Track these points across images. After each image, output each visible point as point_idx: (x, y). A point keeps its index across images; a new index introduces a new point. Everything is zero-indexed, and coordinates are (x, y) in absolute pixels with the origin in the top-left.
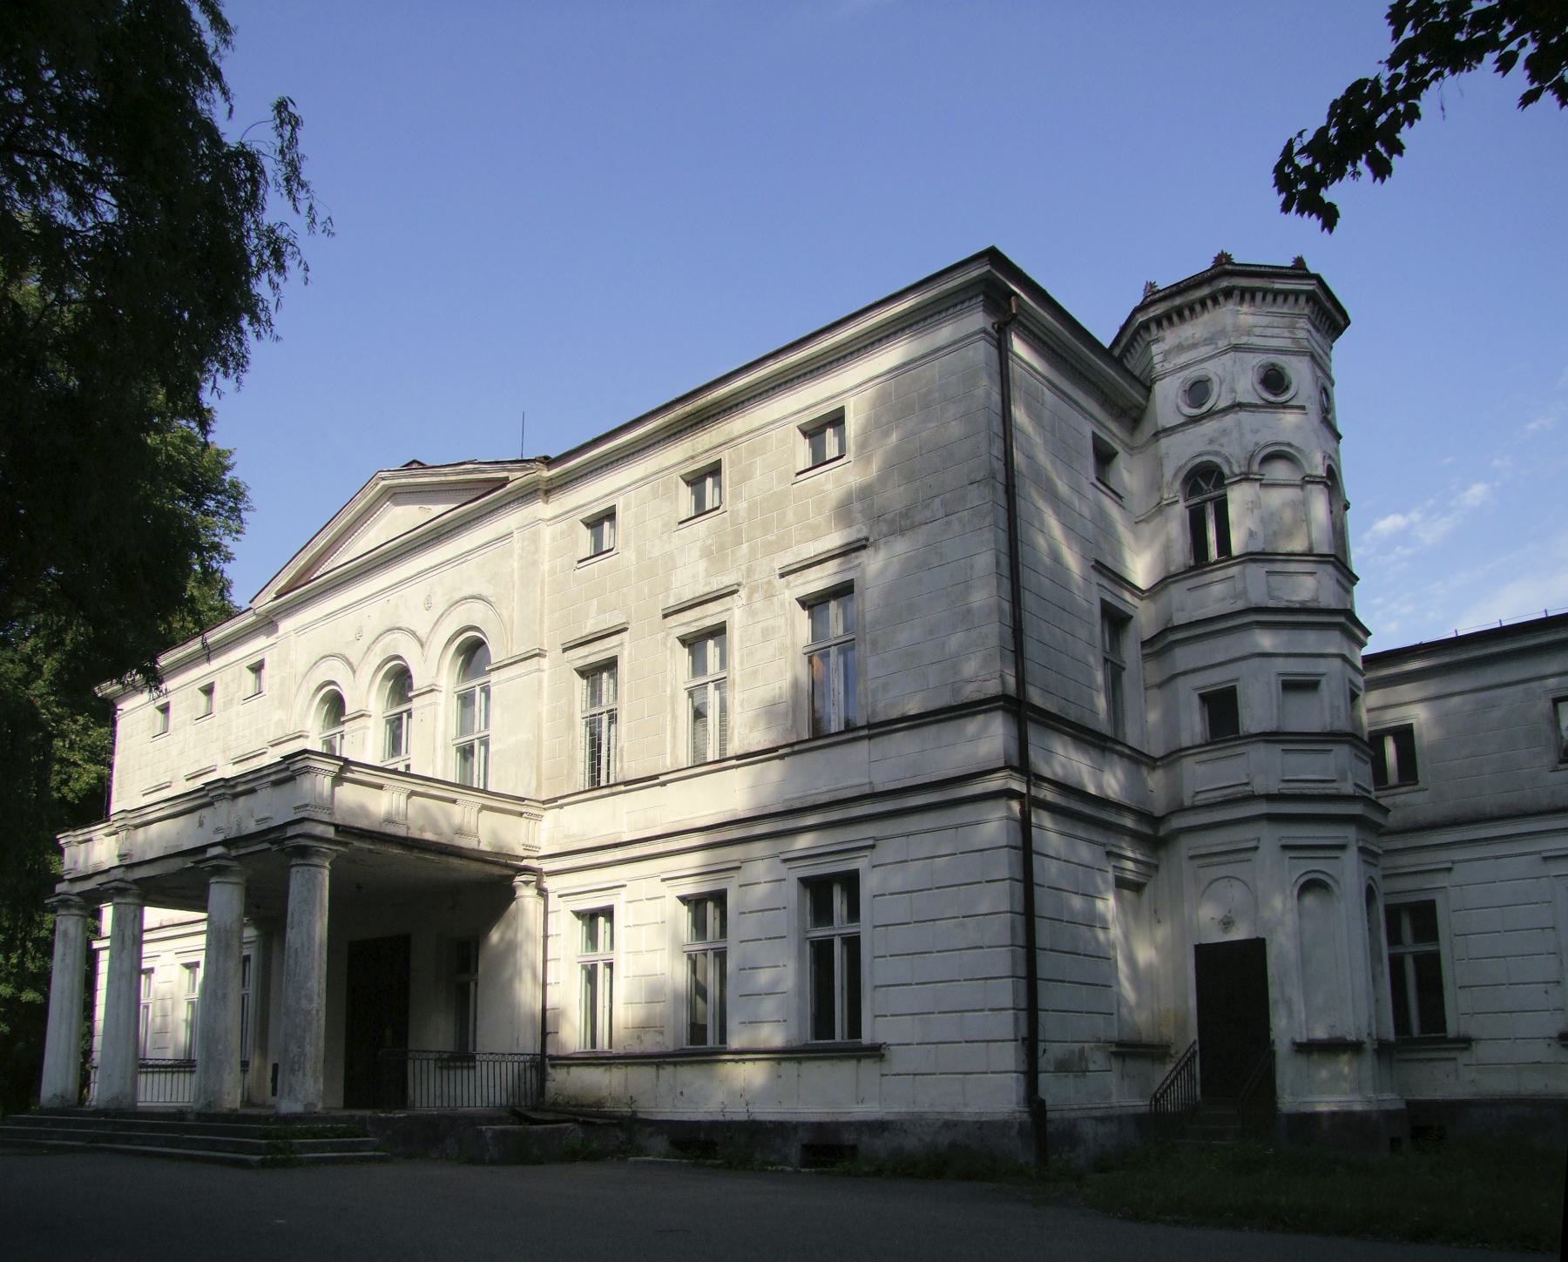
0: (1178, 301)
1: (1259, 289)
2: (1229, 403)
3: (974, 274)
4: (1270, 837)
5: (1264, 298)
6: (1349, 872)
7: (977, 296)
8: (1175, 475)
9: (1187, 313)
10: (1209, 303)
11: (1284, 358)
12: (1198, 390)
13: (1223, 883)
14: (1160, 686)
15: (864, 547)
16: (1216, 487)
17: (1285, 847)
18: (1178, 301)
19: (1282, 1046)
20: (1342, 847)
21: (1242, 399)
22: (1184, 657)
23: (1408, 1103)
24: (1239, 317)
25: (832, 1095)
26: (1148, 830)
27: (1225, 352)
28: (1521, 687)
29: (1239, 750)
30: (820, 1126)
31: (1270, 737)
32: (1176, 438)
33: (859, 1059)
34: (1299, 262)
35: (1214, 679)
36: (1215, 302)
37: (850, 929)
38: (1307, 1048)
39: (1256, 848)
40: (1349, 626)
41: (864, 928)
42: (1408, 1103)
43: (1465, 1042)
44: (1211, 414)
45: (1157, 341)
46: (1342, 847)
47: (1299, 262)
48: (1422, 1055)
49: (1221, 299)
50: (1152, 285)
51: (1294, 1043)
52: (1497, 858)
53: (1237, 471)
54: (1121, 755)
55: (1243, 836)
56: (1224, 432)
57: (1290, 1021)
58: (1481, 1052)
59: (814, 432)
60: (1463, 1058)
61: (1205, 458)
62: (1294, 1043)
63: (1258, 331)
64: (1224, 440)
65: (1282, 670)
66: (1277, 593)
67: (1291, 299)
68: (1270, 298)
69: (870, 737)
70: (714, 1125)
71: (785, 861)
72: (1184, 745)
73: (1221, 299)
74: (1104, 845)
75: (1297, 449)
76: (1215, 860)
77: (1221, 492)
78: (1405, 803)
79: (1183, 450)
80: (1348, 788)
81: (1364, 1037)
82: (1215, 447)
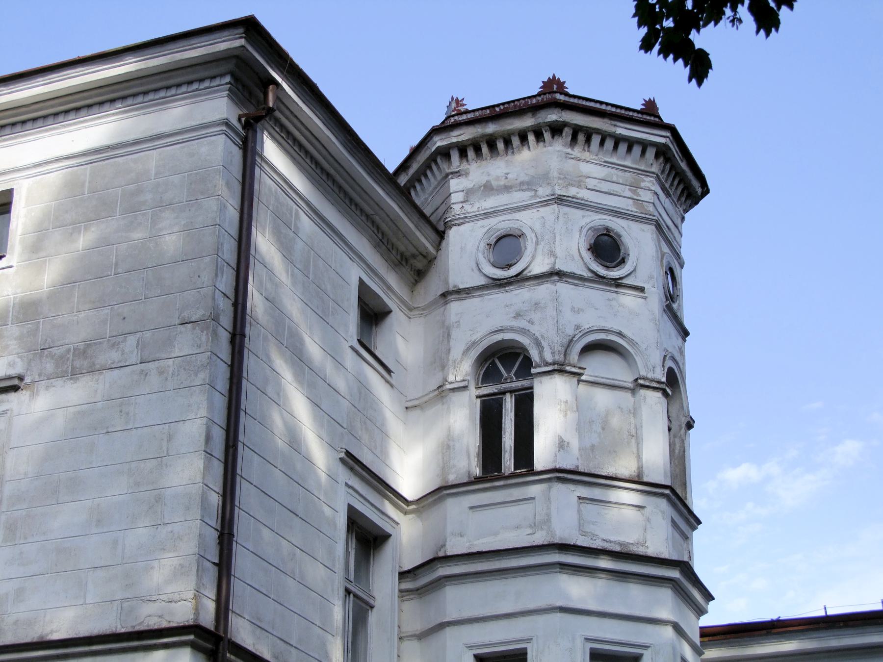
0: (491, 128)
1: (598, 131)
3: (223, 46)
5: (602, 143)
7: (222, 75)
12: (506, 245)
15: (15, 389)
22: (458, 600)
34: (650, 107)
40: (684, 581)
44: (520, 279)
47: (650, 107)
56: (537, 305)
63: (591, 183)
64: (536, 316)
66: (589, 528)
67: (637, 150)
68: (623, 147)
75: (631, 341)
77: (525, 383)
82: (521, 323)
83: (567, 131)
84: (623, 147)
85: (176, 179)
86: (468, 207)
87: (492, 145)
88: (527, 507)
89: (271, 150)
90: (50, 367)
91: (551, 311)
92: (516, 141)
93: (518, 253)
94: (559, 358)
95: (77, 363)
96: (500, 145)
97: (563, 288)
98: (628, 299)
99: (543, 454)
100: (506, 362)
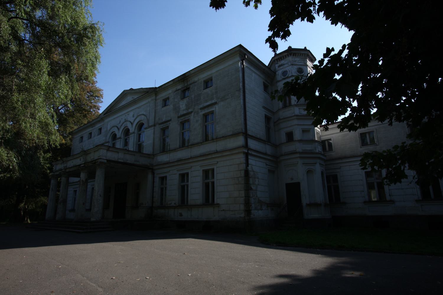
2: (291, 75)
9: (282, 58)
10: (287, 56)
11: (302, 66)
20: (316, 163)
35: (288, 130)
38: (310, 205)
96: (282, 58)
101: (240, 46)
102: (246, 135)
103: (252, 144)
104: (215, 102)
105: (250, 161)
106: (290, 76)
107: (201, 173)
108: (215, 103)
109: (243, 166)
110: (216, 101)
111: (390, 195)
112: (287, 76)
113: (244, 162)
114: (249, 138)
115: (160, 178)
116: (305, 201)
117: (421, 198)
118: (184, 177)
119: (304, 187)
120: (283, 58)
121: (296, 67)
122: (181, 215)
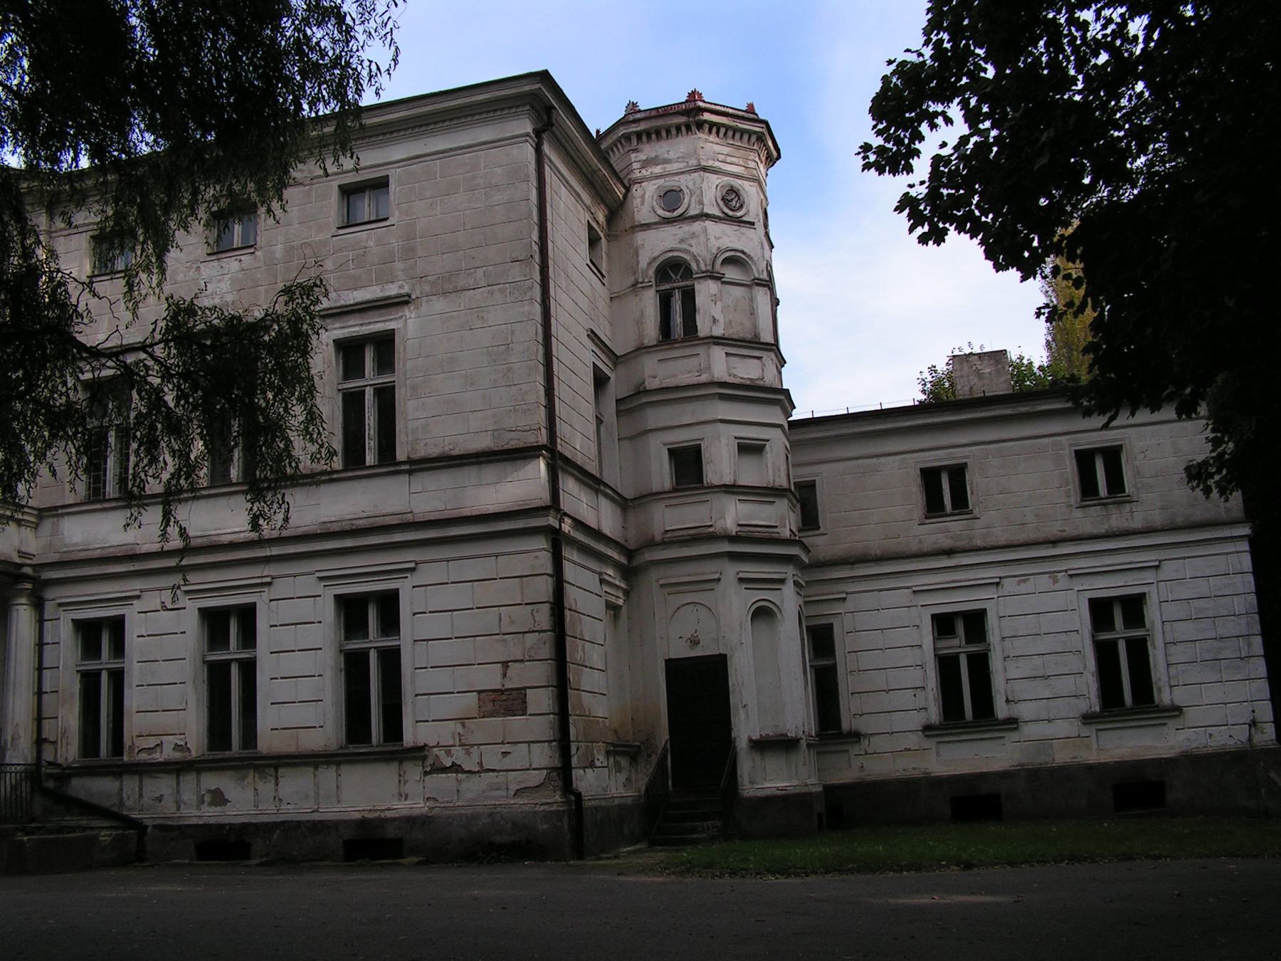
0: (659, 123)
1: (723, 125)
2: (697, 212)
3: (527, 88)
4: (731, 571)
5: (725, 134)
6: (788, 600)
7: (524, 105)
8: (650, 264)
9: (664, 134)
10: (683, 129)
11: (740, 182)
12: (671, 197)
13: (691, 607)
14: (632, 438)
15: (407, 303)
16: (683, 278)
17: (741, 580)
18: (659, 123)
19: (742, 743)
20: (782, 581)
21: (706, 210)
22: (655, 417)
23: (825, 787)
24: (710, 147)
25: (366, 793)
26: (623, 560)
27: (695, 171)
28: (897, 458)
29: (704, 498)
30: (363, 823)
31: (731, 489)
32: (651, 234)
33: (338, 764)
34: (751, 109)
35: (682, 437)
36: (688, 128)
37: (389, 642)
38: (762, 745)
39: (719, 580)
40: (782, 399)
41: (405, 640)
42: (825, 787)
43: (856, 736)
44: (683, 219)
45: (635, 150)
46: (782, 581)
47: (751, 109)
48: (833, 748)
49: (693, 128)
50: (634, 105)
51: (750, 740)
52: (880, 590)
53: (703, 268)
54: (606, 496)
55: (708, 570)
56: (693, 235)
57: (746, 725)
58: (877, 744)
59: (349, 192)
60: (855, 750)
61: (676, 254)
62: (750, 740)
63: (721, 157)
64: (693, 242)
65: (738, 435)
66: (733, 371)
67: (746, 137)
68: (738, 135)
69: (410, 472)
70: (245, 826)
71: (321, 579)
72: (654, 490)
73: (693, 128)
74: (600, 574)
75: (749, 256)
76: (682, 588)
77: (688, 283)
78: (822, 545)
79: (656, 244)
80: (786, 533)
81: (801, 734)
82: (684, 246)
83: (707, 126)
84: (738, 135)
85: (499, 170)
86: (643, 171)
87: (658, 133)
88: (695, 359)
89: (546, 148)
90: (427, 288)
91: (702, 239)
92: (674, 131)
93: (679, 201)
94: (709, 268)
95: (446, 286)
96: (664, 134)
97: (708, 224)
98: (749, 232)
99: (703, 328)
100: (673, 270)
101: (544, 77)
102: (559, 464)
103: (577, 499)
104: (402, 292)
105: (569, 571)
106: (692, 212)
107: (327, 610)
108: (401, 302)
109: (544, 588)
110: (406, 290)
111: (1008, 701)
112: (680, 211)
113: (550, 571)
114: (564, 471)
115: (79, 625)
116: (745, 727)
117: (1097, 709)
118: (228, 625)
119: (742, 674)
120: (668, 132)
121: (715, 180)
122: (218, 798)
